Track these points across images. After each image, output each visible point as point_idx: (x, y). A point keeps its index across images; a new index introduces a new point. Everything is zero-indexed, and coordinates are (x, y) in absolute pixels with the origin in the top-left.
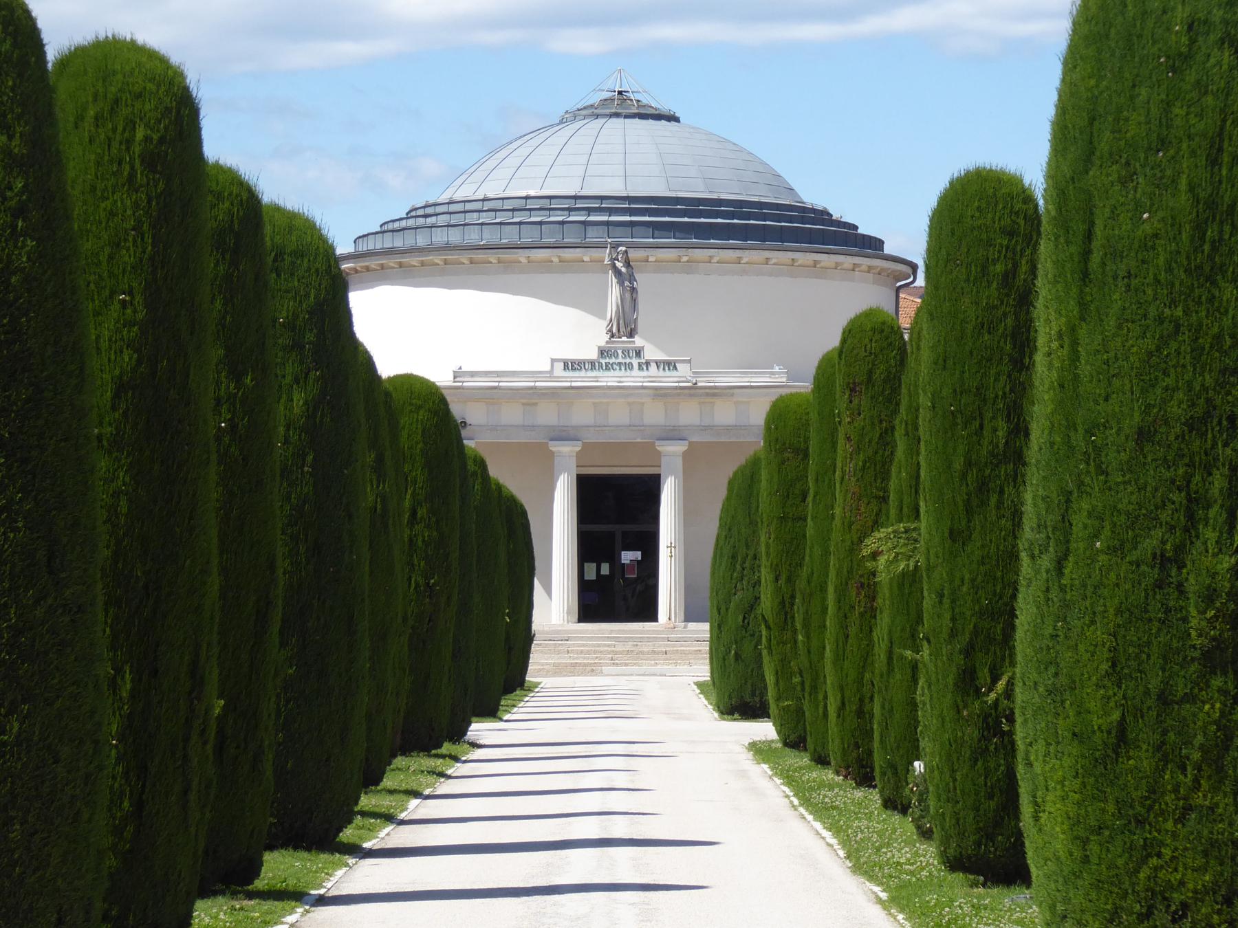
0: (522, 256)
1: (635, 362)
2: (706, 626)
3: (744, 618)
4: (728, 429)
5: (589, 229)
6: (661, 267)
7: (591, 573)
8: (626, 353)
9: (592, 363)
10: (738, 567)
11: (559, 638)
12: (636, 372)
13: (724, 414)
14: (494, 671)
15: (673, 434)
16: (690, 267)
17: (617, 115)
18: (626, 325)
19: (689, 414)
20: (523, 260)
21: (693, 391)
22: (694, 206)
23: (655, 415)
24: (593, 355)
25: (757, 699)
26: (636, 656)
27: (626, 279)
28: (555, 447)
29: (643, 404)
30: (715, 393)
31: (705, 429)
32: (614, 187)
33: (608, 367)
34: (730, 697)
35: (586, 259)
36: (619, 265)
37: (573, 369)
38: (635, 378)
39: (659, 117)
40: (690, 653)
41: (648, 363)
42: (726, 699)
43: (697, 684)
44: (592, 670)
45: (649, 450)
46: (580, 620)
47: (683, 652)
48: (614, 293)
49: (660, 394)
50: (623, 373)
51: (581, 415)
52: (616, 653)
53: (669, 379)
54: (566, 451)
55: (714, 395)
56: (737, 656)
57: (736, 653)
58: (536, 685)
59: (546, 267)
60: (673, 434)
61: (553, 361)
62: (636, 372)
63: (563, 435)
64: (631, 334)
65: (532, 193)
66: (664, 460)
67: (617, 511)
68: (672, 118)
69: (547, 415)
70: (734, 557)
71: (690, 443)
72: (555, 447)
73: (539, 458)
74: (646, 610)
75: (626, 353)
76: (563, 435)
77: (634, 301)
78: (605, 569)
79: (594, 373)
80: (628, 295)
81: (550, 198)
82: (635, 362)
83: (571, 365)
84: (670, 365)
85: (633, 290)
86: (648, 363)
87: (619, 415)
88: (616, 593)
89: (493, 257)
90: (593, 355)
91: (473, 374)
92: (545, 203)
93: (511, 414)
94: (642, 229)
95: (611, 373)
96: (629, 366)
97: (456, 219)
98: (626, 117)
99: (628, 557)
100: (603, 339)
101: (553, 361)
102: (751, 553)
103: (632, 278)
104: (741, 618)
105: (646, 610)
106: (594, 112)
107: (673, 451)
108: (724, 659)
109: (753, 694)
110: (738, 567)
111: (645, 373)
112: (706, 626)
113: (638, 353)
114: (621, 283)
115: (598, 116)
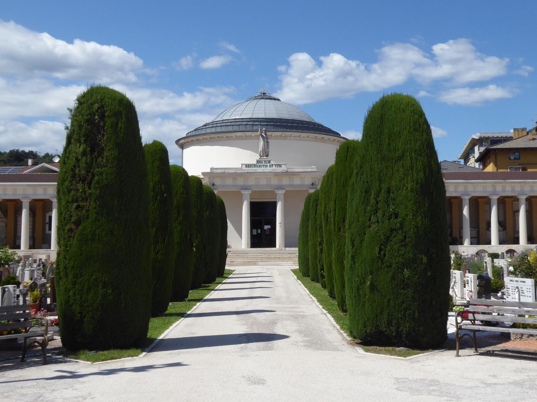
0: (233, 135)
1: (268, 165)
2: (297, 249)
3: (381, 250)
4: (298, 186)
5: (254, 127)
6: (276, 138)
7: (255, 232)
8: (265, 162)
9: (255, 165)
10: (372, 201)
11: (240, 254)
12: (268, 168)
13: (297, 181)
14: (210, 268)
15: (280, 187)
16: (285, 138)
17: (263, 98)
18: (265, 153)
19: (285, 181)
20: (234, 136)
21: (286, 173)
22: (287, 121)
23: (275, 182)
24: (255, 162)
25: (393, 329)
26: (269, 259)
27: (266, 140)
28: (243, 192)
29: (271, 178)
30: (294, 174)
31: (291, 186)
32: (262, 116)
33: (260, 166)
34: (365, 326)
35: (253, 135)
36: (263, 134)
37: (249, 167)
38: (268, 169)
39: (275, 99)
40: (287, 258)
41: (272, 165)
42: (361, 326)
43: (292, 270)
44: (254, 264)
45: (273, 193)
46: (251, 247)
47: (284, 258)
48: (261, 143)
49: (276, 174)
50: (264, 168)
51: (251, 182)
52: (262, 258)
53: (279, 170)
54: (246, 193)
55: (294, 175)
56: (373, 287)
57: (372, 284)
58: (231, 272)
59: (240, 138)
60: (280, 187)
61: (242, 164)
62: (268, 168)
63: (246, 188)
64: (267, 156)
65: (237, 118)
66: (278, 196)
67: (262, 216)
68: (278, 100)
69: (240, 182)
70: (367, 192)
71: (286, 191)
72: (243, 192)
73: (238, 197)
74: (272, 243)
75: (265, 162)
76: (246, 188)
77: (268, 146)
78: (259, 231)
79: (255, 168)
80: (266, 144)
81: (242, 119)
82: (268, 165)
83: (248, 166)
84: (280, 166)
85: (268, 142)
86: (272, 165)
87: (263, 182)
88: (262, 238)
89: (224, 135)
90: (255, 162)
91: (217, 169)
92: (241, 120)
93: (229, 182)
94: (270, 126)
95: (261, 168)
96: (267, 166)
97: (214, 125)
98: (266, 99)
99: (266, 227)
100: (258, 157)
101: (242, 164)
102: (384, 186)
103: (267, 138)
104: (377, 249)
105: (272, 243)
106: (256, 98)
107: (281, 192)
108: (358, 289)
109: (389, 323)
110: (372, 201)
111: (271, 168)
112: (297, 249)
113: (269, 162)
114: (264, 140)
115: (257, 99)
